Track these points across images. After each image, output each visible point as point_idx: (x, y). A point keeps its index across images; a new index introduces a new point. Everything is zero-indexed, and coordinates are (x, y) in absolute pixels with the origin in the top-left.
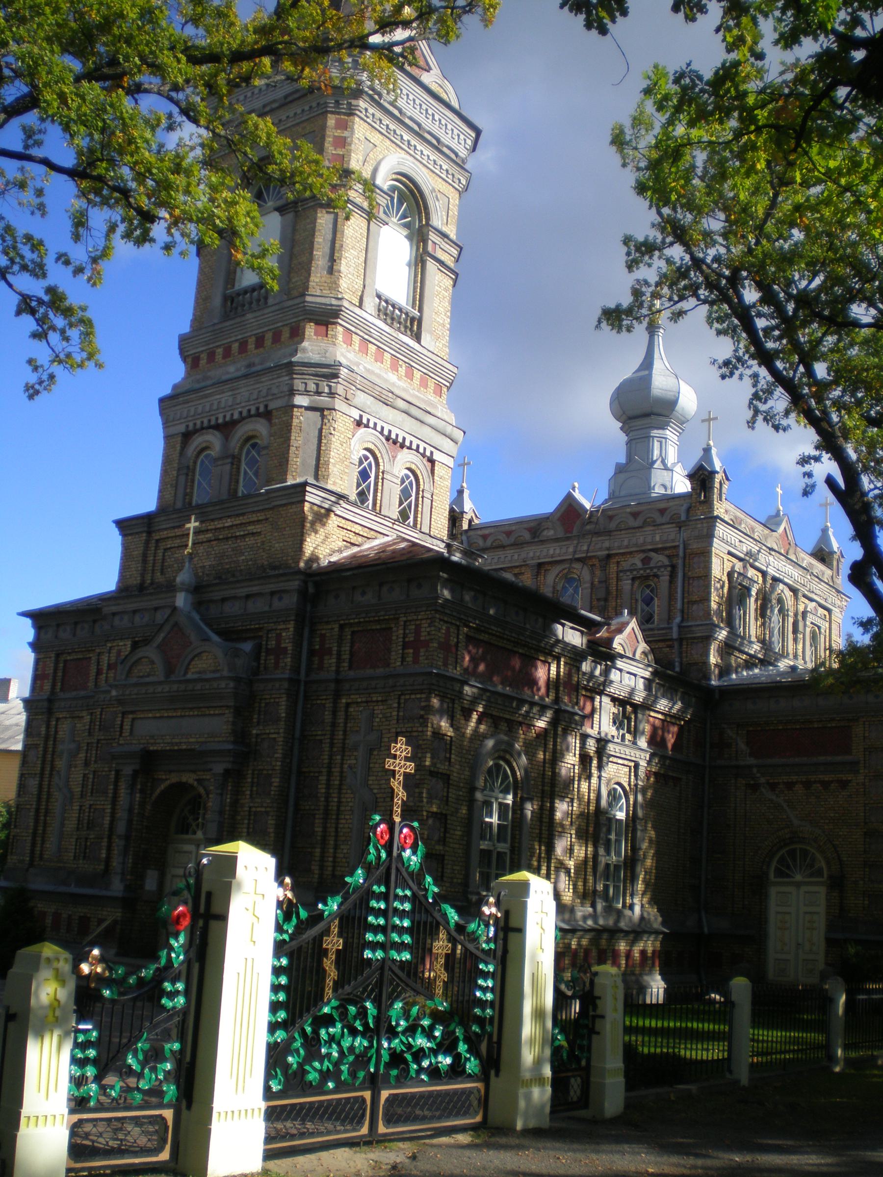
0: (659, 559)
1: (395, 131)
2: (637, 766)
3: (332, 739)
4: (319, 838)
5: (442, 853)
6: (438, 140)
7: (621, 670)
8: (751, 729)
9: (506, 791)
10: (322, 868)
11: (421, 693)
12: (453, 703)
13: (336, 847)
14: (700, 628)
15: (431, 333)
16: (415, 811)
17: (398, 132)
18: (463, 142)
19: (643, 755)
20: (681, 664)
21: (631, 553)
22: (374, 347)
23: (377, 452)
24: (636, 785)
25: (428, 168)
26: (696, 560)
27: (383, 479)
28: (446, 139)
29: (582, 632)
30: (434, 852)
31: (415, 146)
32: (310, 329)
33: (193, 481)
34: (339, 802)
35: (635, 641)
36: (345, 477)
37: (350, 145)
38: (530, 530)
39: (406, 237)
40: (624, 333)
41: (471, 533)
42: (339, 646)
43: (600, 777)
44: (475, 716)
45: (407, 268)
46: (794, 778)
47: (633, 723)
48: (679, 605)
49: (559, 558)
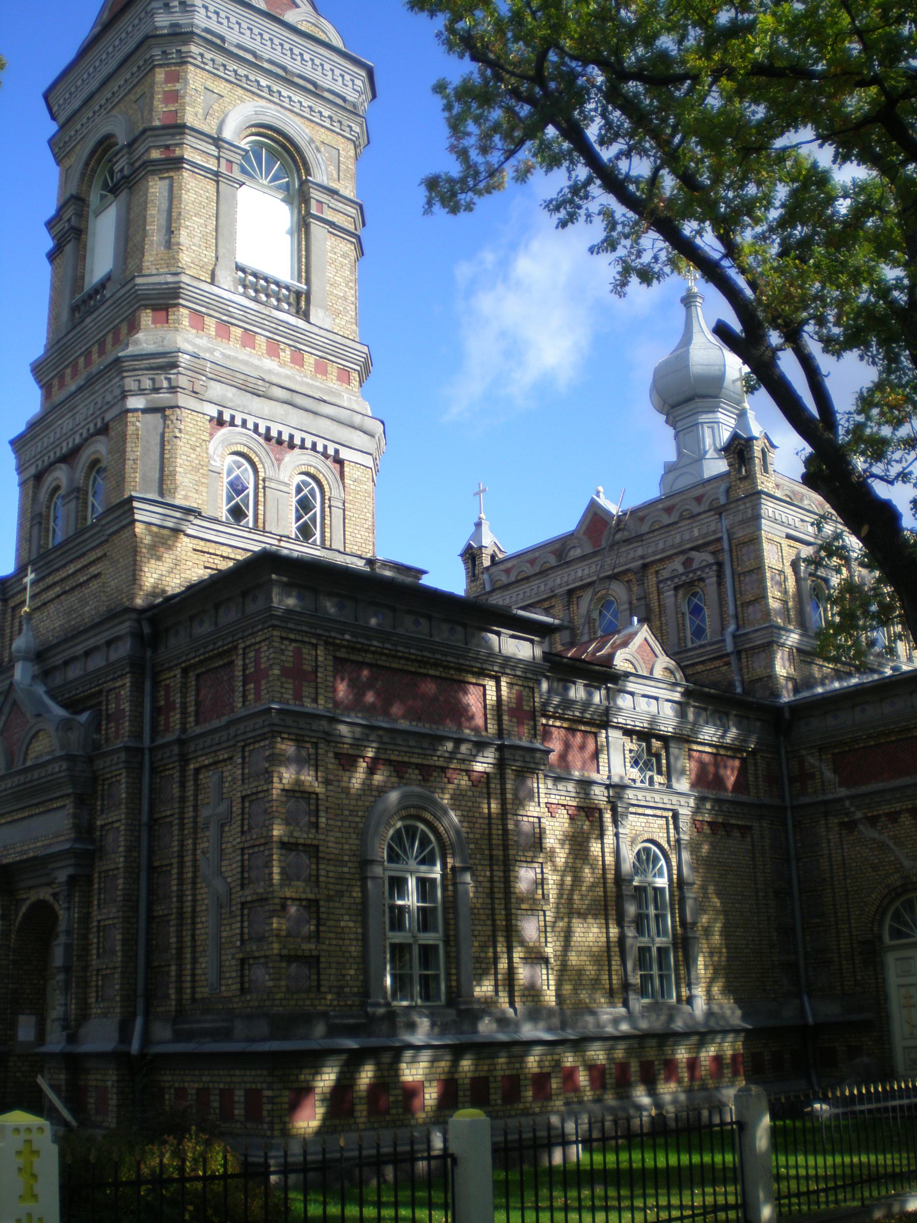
0: (702, 558)
1: (247, 77)
2: (676, 816)
3: (182, 819)
4: (174, 951)
5: (315, 953)
6: (314, 84)
7: (632, 694)
8: (836, 751)
9: (428, 861)
10: (180, 990)
11: (264, 739)
12: (317, 748)
13: (194, 961)
14: (759, 633)
15: (326, 308)
16: (266, 899)
17: (252, 77)
18: (350, 84)
19: (683, 800)
20: (743, 682)
21: (669, 557)
22: (240, 331)
23: (253, 456)
24: (678, 841)
25: (303, 117)
26: (744, 551)
27: (264, 488)
28: (325, 82)
29: (532, 641)
30: (300, 953)
31: (279, 92)
32: (146, 318)
33: (47, 531)
34: (194, 901)
35: (651, 655)
36: (201, 489)
37: (183, 97)
38: (554, 552)
39: (283, 200)
40: (463, 215)
41: (493, 569)
42: (184, 696)
43: (617, 835)
44: (362, 765)
45: (289, 237)
46: (898, 807)
47: (664, 761)
48: (731, 610)
49: (589, 580)
